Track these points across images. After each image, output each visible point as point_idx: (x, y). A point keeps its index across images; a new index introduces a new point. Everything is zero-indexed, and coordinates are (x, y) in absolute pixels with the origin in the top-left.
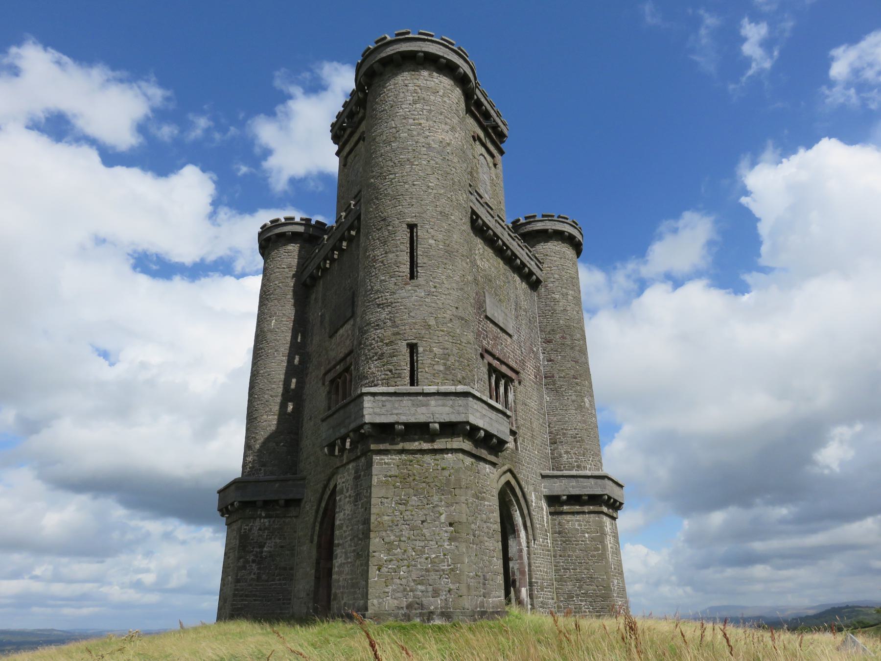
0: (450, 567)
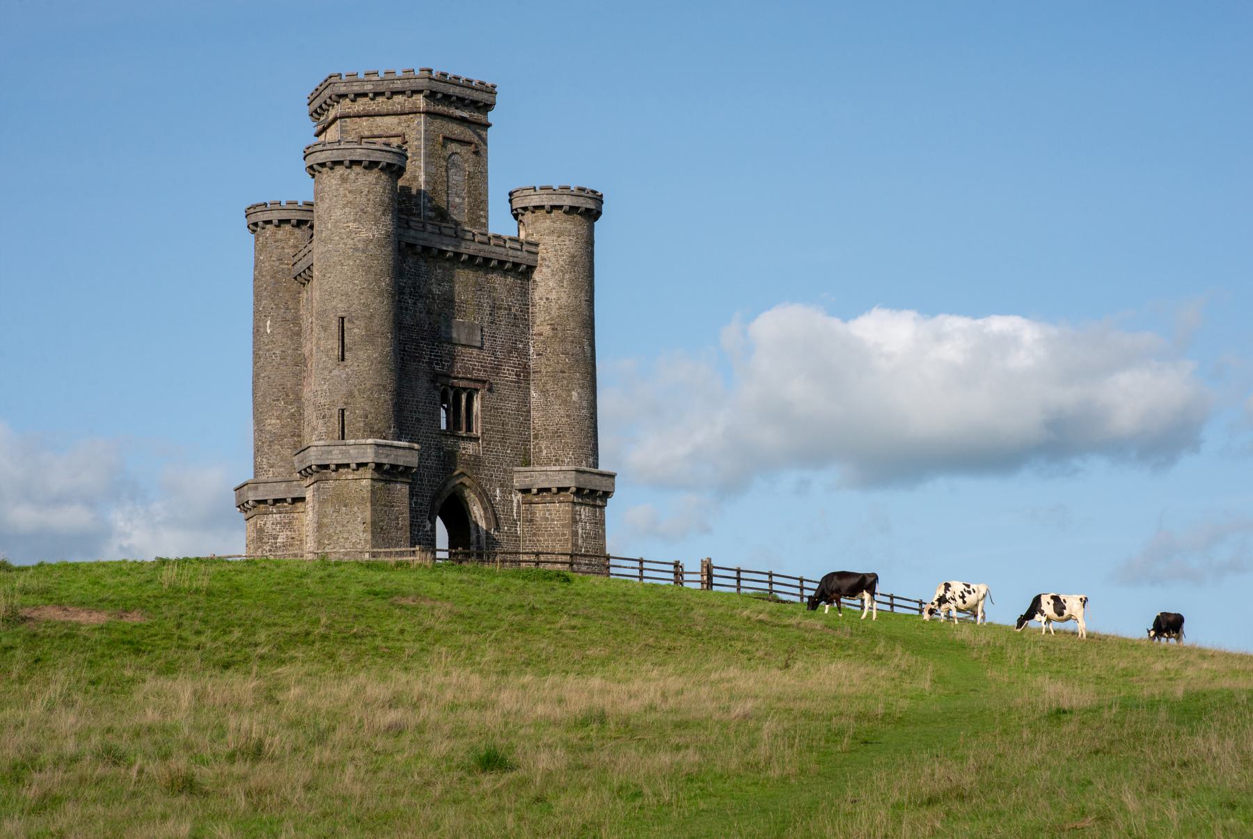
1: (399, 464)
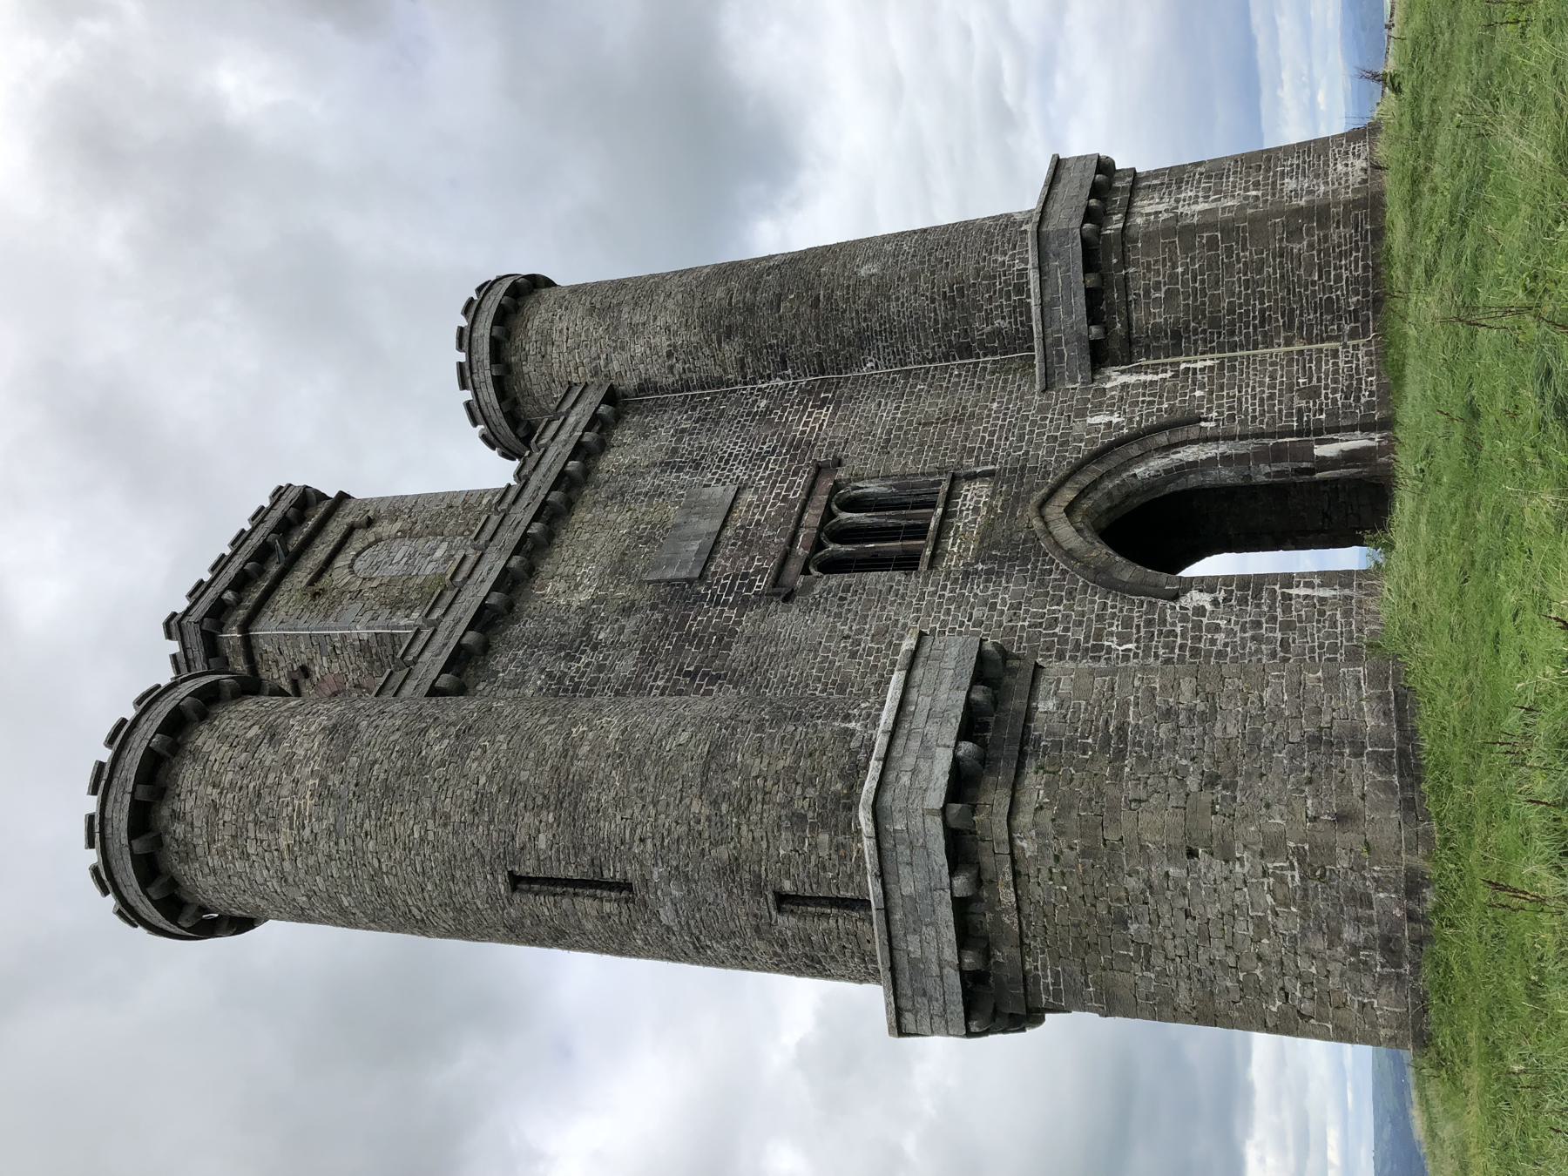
0: (1296, 864)
1: (961, 703)
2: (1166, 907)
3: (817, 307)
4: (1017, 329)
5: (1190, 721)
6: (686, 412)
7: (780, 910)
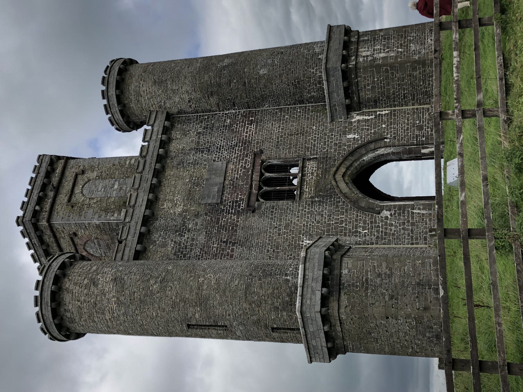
1: (321, 275)
2: (381, 330)
3: (245, 86)
4: (320, 96)
5: (386, 277)
6: (199, 124)
7: (273, 331)
